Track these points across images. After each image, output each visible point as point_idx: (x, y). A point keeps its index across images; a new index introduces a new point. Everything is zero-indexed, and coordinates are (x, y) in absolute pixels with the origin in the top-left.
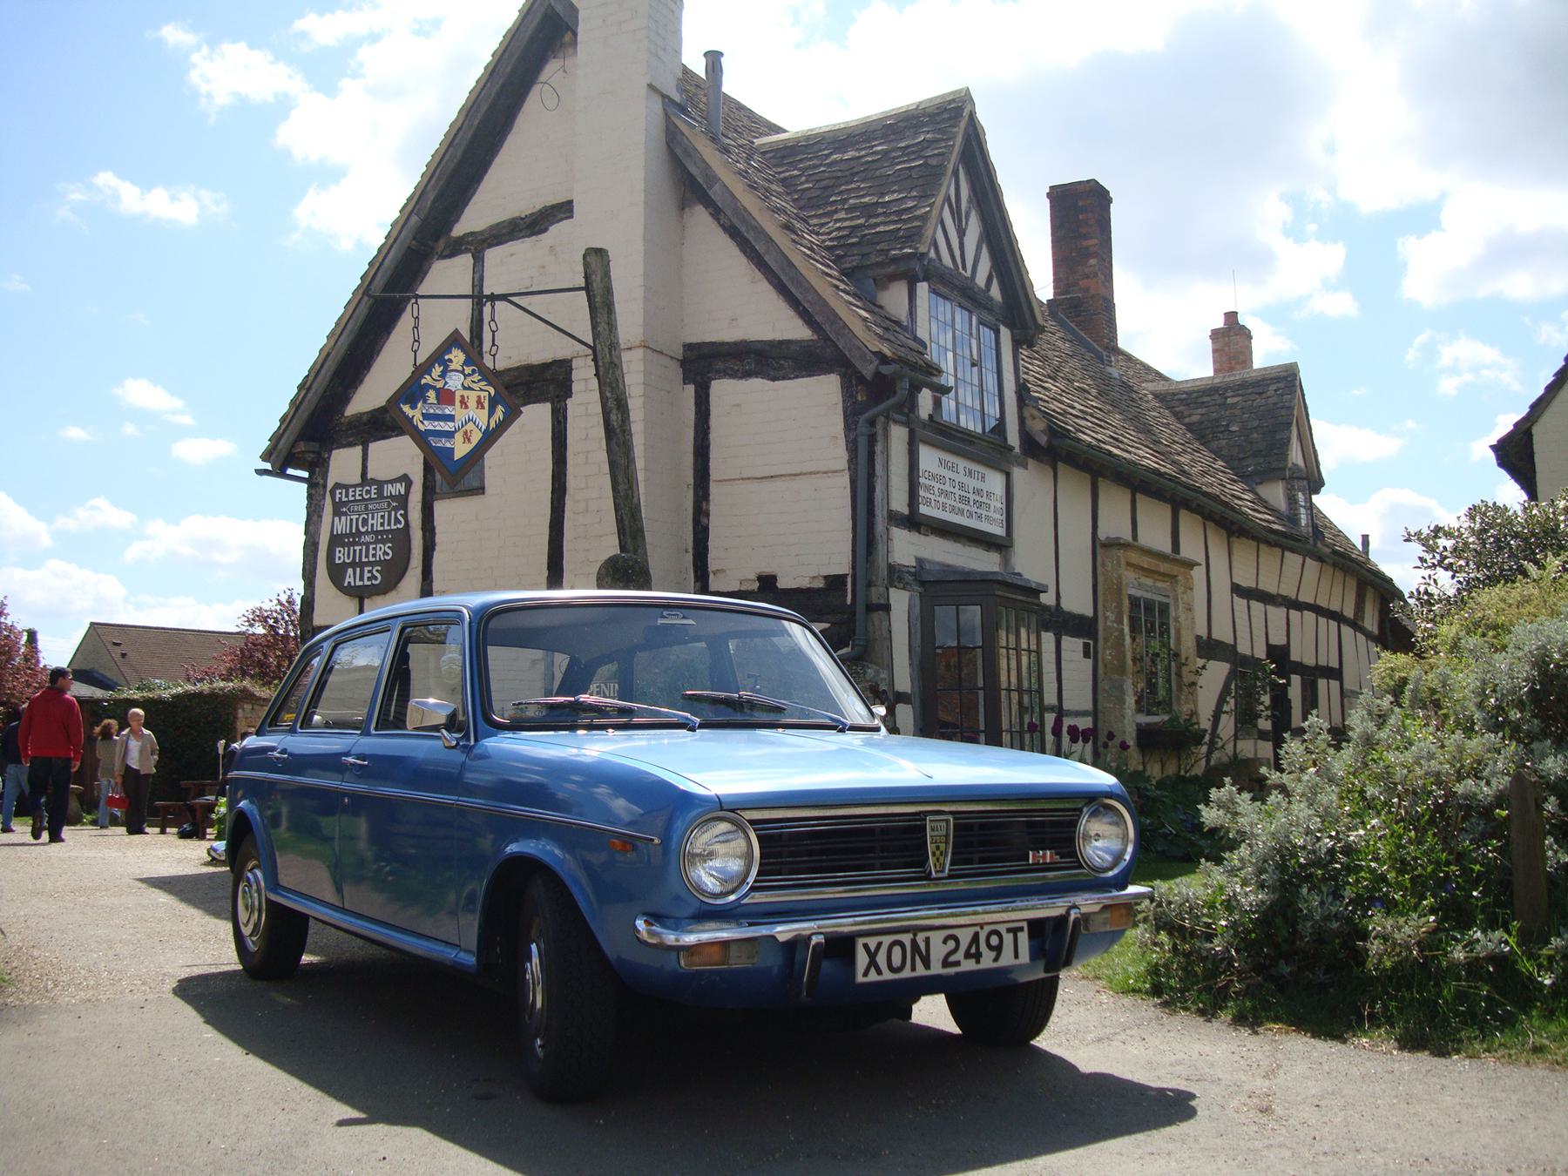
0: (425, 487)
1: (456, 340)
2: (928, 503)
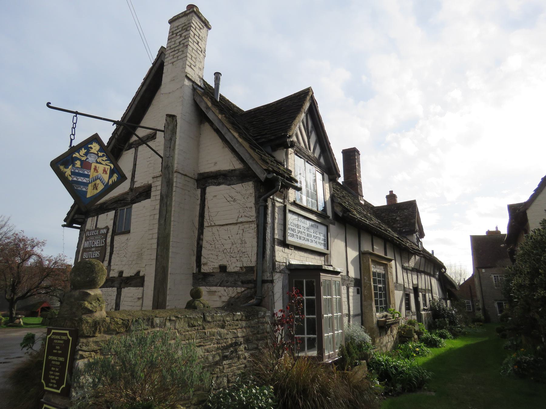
0: (113, 230)
1: (96, 139)
2: (293, 236)
